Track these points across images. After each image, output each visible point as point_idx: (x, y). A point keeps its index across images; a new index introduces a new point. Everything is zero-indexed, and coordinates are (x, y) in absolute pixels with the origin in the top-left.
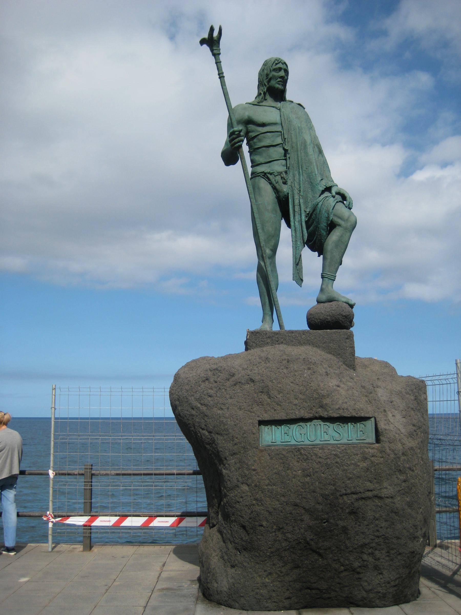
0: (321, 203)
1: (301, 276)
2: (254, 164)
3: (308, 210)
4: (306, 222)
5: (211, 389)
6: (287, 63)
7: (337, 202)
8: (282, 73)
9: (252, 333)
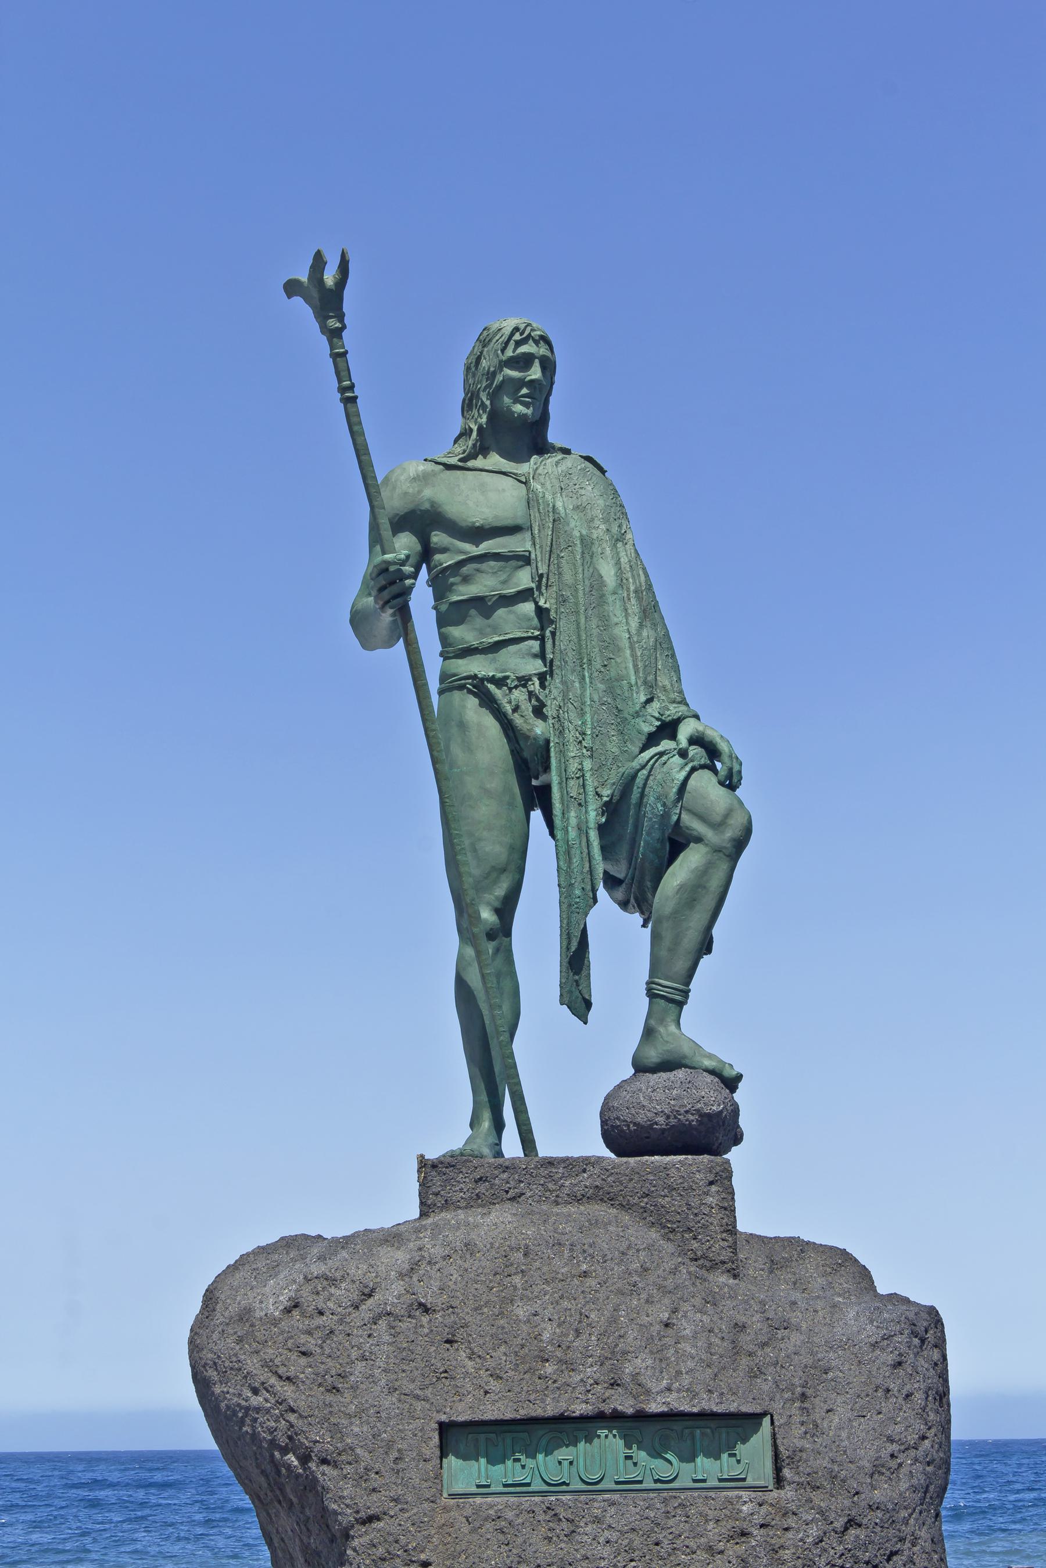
0: (645, 772)
1: (584, 992)
2: (451, 651)
3: (606, 792)
4: (601, 829)
5: (309, 1333)
6: (551, 338)
7: (694, 770)
8: (535, 373)
9: (434, 1166)
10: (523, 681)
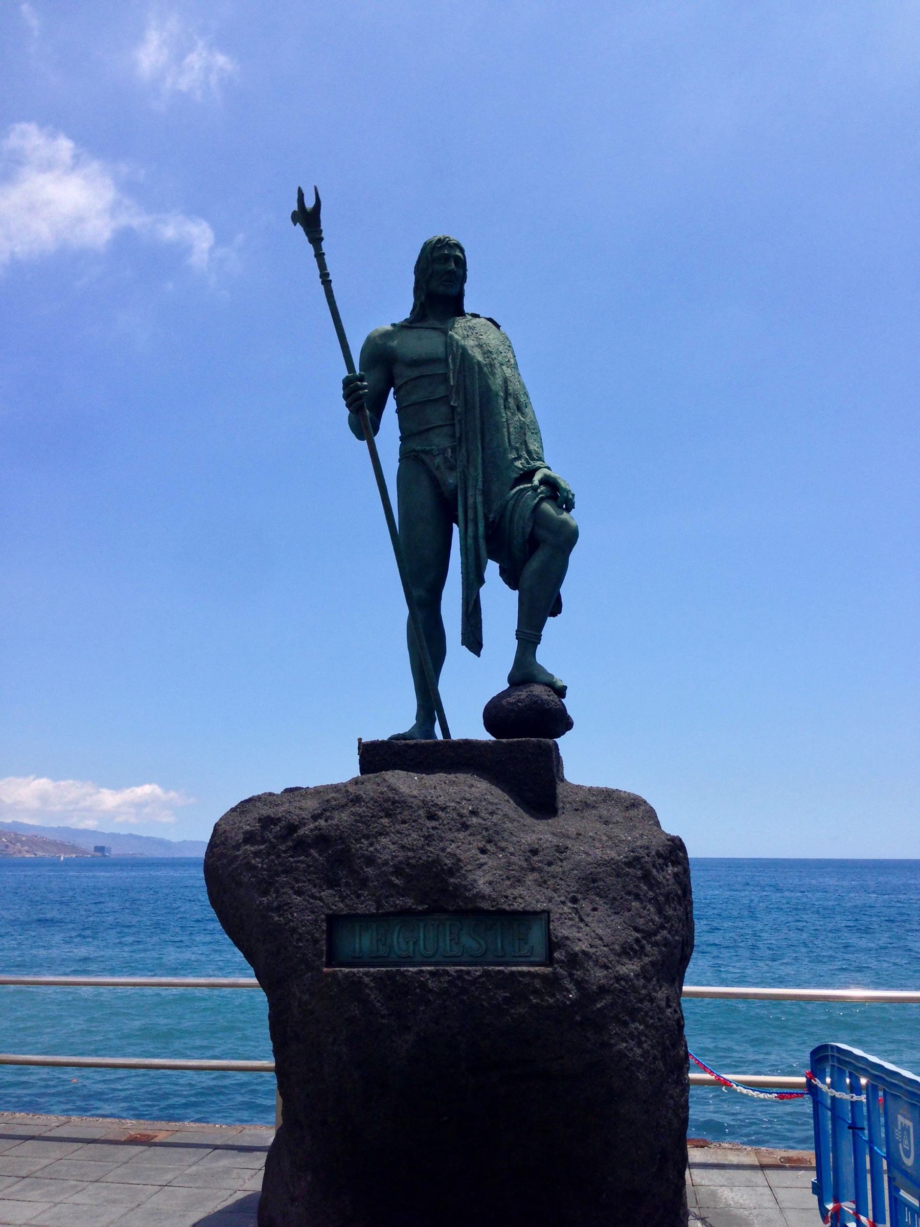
10: (443, 451)
